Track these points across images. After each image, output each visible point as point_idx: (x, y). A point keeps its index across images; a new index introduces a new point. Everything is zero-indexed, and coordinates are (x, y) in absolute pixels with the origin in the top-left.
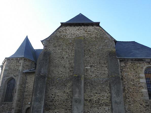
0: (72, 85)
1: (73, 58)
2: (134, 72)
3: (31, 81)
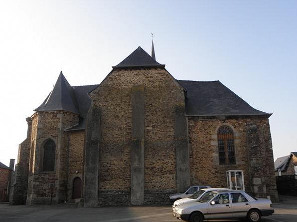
0: (130, 151)
1: (130, 116)
2: (205, 133)
3: (78, 144)
